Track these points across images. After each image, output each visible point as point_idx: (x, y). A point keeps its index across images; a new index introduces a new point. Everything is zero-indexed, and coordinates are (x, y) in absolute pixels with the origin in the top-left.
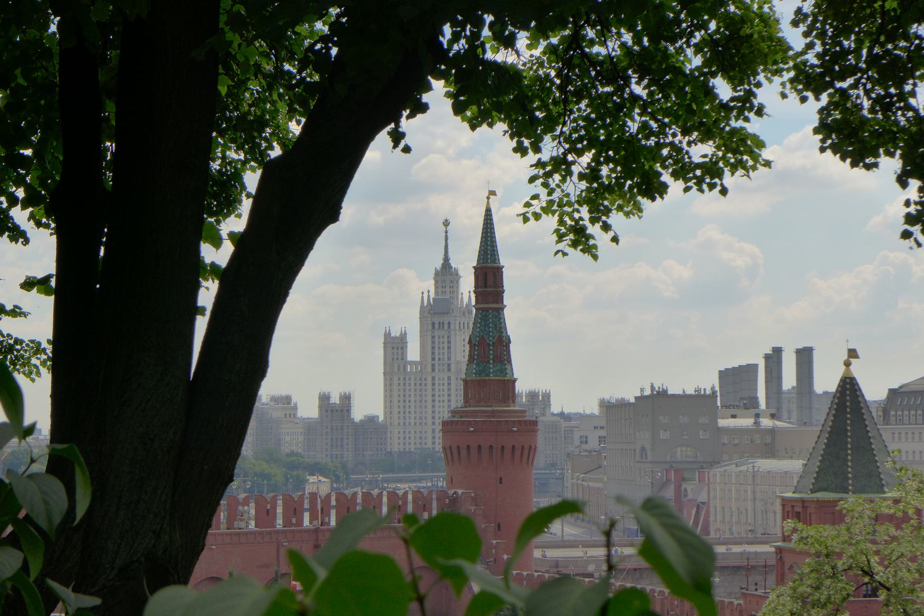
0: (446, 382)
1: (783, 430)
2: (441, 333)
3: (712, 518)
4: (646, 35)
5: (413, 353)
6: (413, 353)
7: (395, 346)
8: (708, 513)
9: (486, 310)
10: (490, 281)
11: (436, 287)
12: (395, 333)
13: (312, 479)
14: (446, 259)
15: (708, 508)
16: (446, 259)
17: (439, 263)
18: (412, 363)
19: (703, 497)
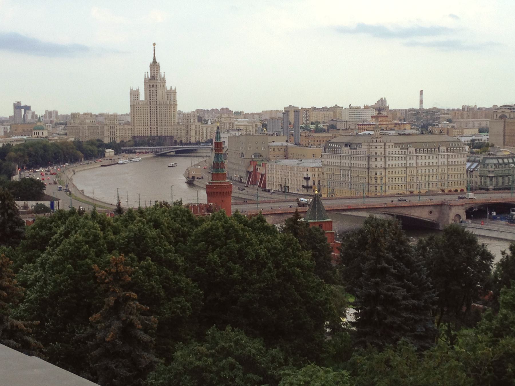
0: (155, 109)
1: (291, 147)
2: (153, 89)
3: (267, 180)
4: (354, 305)
5: (142, 97)
6: (142, 97)
7: (134, 94)
8: (265, 178)
9: (218, 154)
10: (219, 146)
11: (151, 70)
12: (135, 89)
13: (108, 150)
14: (154, 59)
15: (266, 176)
16: (154, 59)
17: (151, 61)
18: (141, 101)
19: (264, 172)
